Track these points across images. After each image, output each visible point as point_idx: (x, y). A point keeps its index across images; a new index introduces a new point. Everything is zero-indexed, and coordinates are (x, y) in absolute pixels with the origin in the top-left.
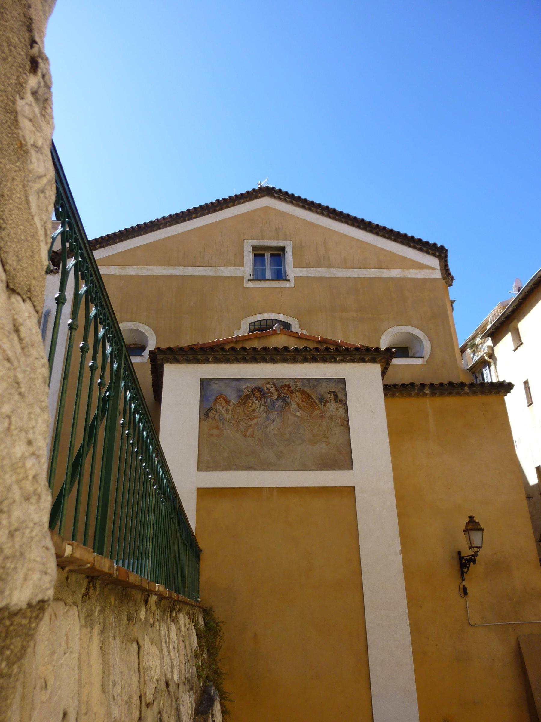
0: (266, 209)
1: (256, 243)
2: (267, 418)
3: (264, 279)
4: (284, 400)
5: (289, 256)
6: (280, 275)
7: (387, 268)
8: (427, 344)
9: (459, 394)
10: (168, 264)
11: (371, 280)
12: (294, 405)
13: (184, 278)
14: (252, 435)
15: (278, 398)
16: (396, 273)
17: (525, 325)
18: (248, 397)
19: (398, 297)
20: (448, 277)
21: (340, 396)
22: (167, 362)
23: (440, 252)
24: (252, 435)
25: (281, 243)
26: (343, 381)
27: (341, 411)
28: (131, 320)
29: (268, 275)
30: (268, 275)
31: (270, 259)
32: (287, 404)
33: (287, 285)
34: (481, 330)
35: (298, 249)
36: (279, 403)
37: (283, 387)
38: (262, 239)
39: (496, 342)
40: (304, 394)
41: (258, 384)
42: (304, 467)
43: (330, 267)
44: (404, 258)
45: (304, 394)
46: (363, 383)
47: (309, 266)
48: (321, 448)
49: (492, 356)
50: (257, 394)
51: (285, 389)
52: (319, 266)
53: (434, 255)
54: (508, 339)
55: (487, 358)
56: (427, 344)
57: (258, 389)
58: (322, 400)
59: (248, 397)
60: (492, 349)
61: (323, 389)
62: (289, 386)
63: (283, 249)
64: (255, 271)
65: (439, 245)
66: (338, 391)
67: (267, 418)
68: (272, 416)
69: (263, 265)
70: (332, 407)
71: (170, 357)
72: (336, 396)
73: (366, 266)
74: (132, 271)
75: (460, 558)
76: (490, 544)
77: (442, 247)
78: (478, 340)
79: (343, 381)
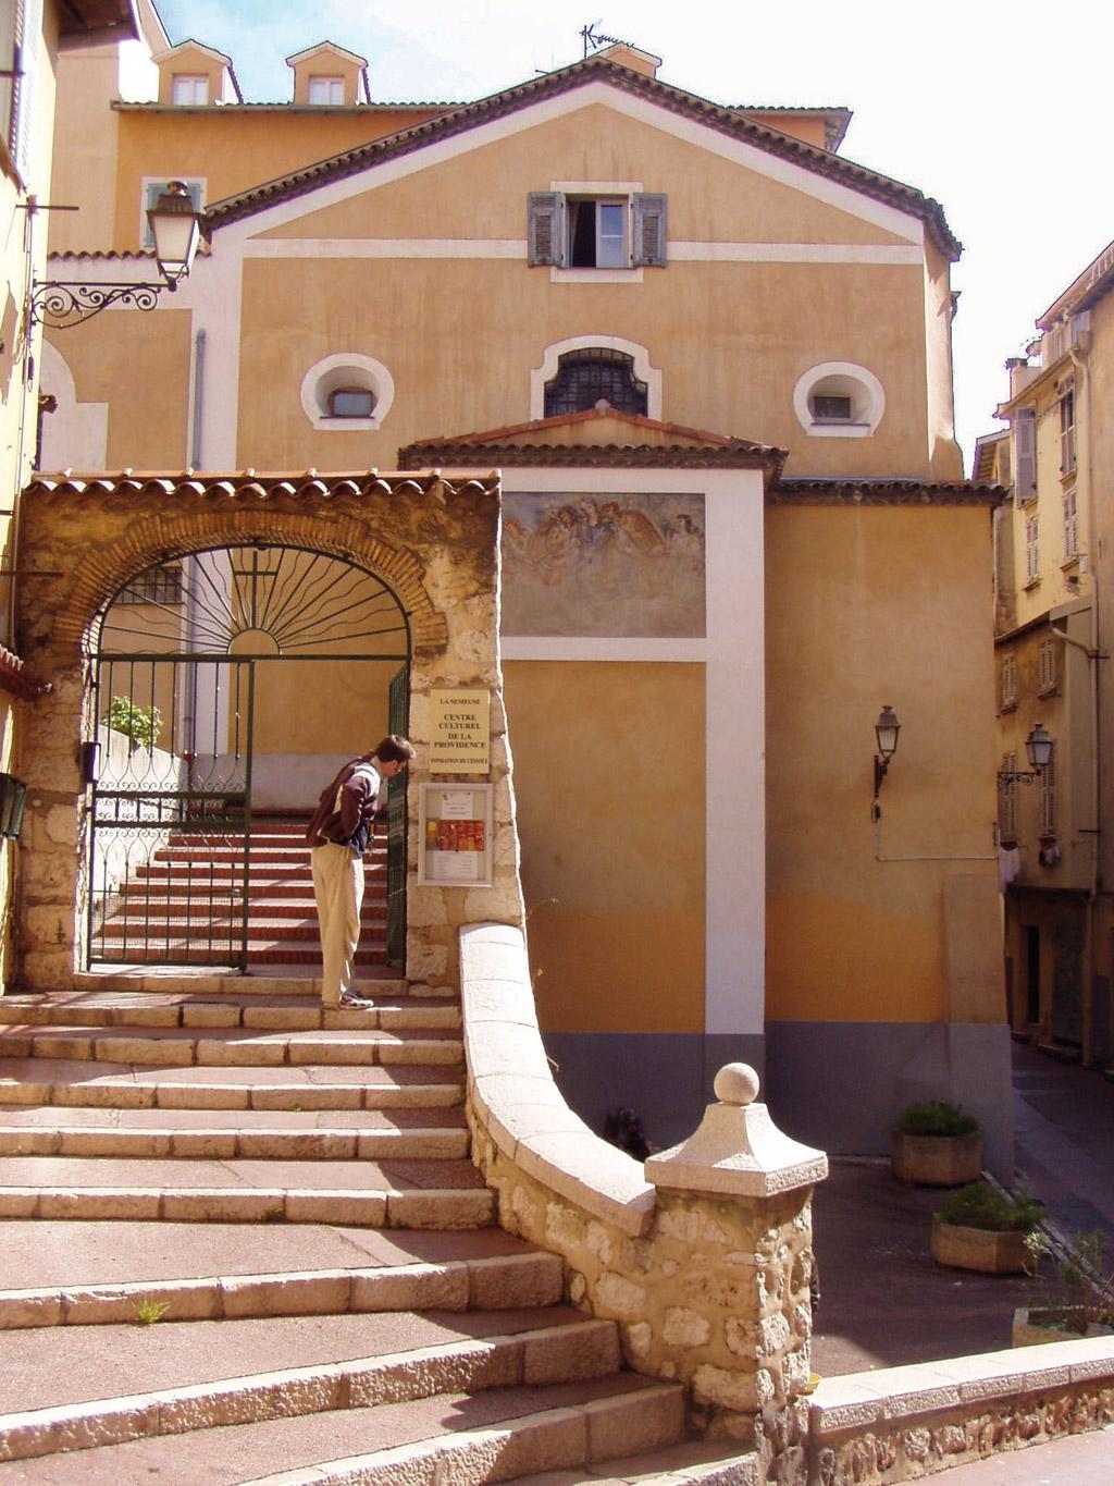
0: (595, 110)
2: (581, 557)
4: (607, 527)
12: (622, 536)
16: (837, 254)
18: (553, 522)
20: (944, 247)
21: (695, 522)
23: (928, 212)
27: (695, 546)
32: (612, 534)
36: (600, 533)
40: (640, 518)
41: (568, 501)
42: (633, 632)
45: (640, 518)
46: (734, 506)
50: (566, 518)
51: (610, 509)
57: (569, 510)
58: (668, 529)
59: (553, 522)
61: (671, 511)
62: (615, 506)
66: (690, 515)
68: (588, 553)
70: (682, 540)
72: (689, 523)
74: (344, 249)
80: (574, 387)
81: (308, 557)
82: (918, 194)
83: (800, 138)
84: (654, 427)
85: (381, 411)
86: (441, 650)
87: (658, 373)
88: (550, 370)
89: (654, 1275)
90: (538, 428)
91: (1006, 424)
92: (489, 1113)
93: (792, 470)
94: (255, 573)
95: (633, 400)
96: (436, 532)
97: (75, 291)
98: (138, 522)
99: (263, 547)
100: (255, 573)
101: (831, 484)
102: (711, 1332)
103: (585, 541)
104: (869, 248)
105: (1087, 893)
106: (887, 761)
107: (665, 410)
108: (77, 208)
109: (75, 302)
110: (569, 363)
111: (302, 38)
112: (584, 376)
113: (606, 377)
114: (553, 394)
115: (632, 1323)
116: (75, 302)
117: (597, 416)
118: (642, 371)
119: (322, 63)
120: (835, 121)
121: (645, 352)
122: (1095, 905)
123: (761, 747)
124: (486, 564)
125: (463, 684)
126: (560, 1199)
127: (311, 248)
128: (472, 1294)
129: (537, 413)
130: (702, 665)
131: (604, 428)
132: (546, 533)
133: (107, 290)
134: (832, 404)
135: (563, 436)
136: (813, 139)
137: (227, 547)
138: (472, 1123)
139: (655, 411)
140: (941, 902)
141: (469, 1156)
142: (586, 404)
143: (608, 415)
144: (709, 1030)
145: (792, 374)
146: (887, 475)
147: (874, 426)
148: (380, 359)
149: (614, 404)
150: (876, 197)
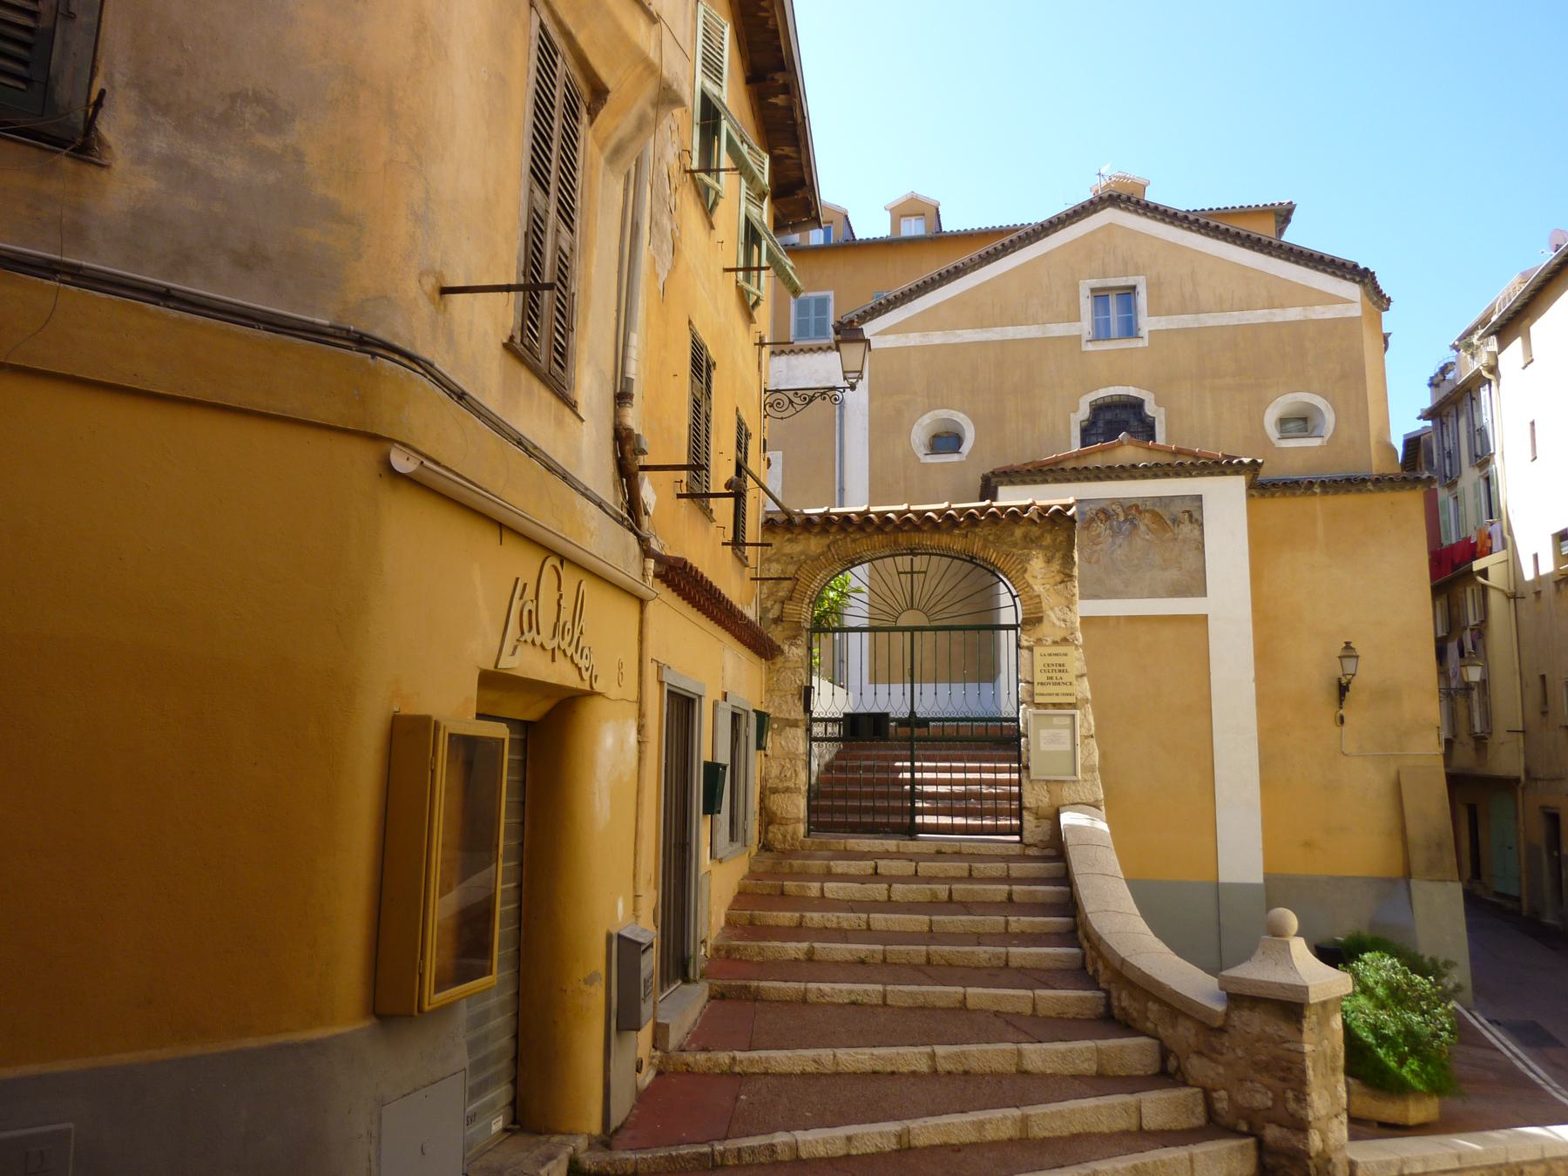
0: (1110, 228)
1: (1097, 283)
2: (1114, 543)
3: (1108, 338)
4: (1132, 522)
5: (1142, 299)
6: (1130, 330)
7: (1282, 306)
8: (1330, 418)
9: (1360, 491)
10: (980, 324)
11: (1255, 328)
12: (1143, 528)
13: (1003, 344)
14: (1098, 561)
15: (1126, 520)
16: (1293, 314)
17: (1542, 328)
18: (1092, 520)
19: (1296, 350)
20: (1380, 300)
21: (1196, 515)
22: (1002, 484)
23: (1362, 276)
24: (1098, 561)
25: (1130, 281)
26: (1199, 498)
27: (1196, 532)
28: (943, 407)
29: (1114, 327)
30: (1114, 327)
31: (1118, 304)
32: (1135, 527)
33: (1140, 344)
34: (1483, 322)
35: (1155, 287)
36: (1127, 526)
37: (1130, 507)
38: (1105, 276)
39: (1503, 346)
40: (1155, 514)
41: (1103, 505)
42: (1153, 594)
43: (1198, 311)
44: (1308, 290)
45: (1155, 514)
46: (1224, 500)
47: (1169, 313)
48: (1172, 574)
49: (1493, 369)
50: (1102, 516)
51: (1133, 509)
52: (1183, 311)
53: (1354, 281)
54: (1517, 345)
55: (1485, 373)
56: (1330, 418)
57: (1104, 511)
58: (1176, 521)
59: (1092, 520)
60: (1495, 356)
61: (1176, 509)
62: (1137, 507)
63: (1134, 288)
64: (1096, 324)
65: (1362, 267)
66: (1192, 511)
67: (1114, 543)
68: (1119, 540)
69: (1107, 312)
70: (1186, 529)
71: (1006, 479)
72: (1191, 516)
73: (1250, 308)
74: (937, 338)
75: (1340, 684)
76: (1366, 675)
77: (1366, 269)
78: (1475, 339)
79: (1199, 498)
80: (1101, 424)
81: (946, 561)
82: (1356, 266)
83: (1259, 229)
84: (1159, 449)
85: (966, 447)
86: (1040, 620)
87: (1162, 410)
88: (1084, 412)
89: (1229, 1057)
90: (1078, 456)
91: (1429, 423)
92: (1100, 938)
93: (1265, 474)
94: (912, 573)
95: (1146, 429)
96: (1029, 542)
97: (791, 394)
98: (834, 542)
99: (916, 555)
100: (912, 573)
101: (1297, 482)
102: (1274, 1100)
103: (1115, 533)
104: (1318, 308)
105: (1518, 780)
106: (1349, 682)
107: (1168, 436)
108: (1543, 677)
109: (791, 402)
110: (1099, 409)
111: (898, 194)
112: (1109, 416)
113: (1123, 416)
114: (1087, 434)
115: (1215, 1090)
116: (791, 402)
117: (1121, 444)
118: (1150, 409)
119: (912, 207)
120: (1283, 215)
121: (1152, 396)
122: (1524, 788)
123: (1252, 674)
124: (1068, 560)
125: (1055, 643)
126: (1157, 1000)
127: (914, 339)
128: (1100, 1065)
129: (1076, 447)
130: (1206, 616)
131: (1127, 451)
132: (1088, 528)
133: (811, 393)
134: (1299, 422)
135: (1097, 461)
136: (1265, 229)
137: (893, 556)
138: (1085, 944)
139: (1161, 438)
140: (1397, 787)
141: (1084, 968)
142: (1111, 433)
143: (1130, 443)
144: (1225, 877)
145: (1263, 405)
146: (1338, 472)
147: (1327, 437)
148: (965, 413)
149: (1132, 434)
150: (1324, 271)
